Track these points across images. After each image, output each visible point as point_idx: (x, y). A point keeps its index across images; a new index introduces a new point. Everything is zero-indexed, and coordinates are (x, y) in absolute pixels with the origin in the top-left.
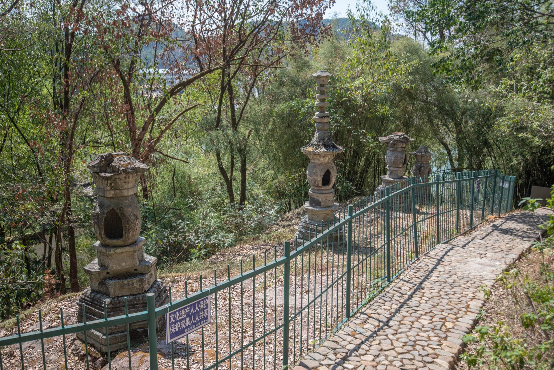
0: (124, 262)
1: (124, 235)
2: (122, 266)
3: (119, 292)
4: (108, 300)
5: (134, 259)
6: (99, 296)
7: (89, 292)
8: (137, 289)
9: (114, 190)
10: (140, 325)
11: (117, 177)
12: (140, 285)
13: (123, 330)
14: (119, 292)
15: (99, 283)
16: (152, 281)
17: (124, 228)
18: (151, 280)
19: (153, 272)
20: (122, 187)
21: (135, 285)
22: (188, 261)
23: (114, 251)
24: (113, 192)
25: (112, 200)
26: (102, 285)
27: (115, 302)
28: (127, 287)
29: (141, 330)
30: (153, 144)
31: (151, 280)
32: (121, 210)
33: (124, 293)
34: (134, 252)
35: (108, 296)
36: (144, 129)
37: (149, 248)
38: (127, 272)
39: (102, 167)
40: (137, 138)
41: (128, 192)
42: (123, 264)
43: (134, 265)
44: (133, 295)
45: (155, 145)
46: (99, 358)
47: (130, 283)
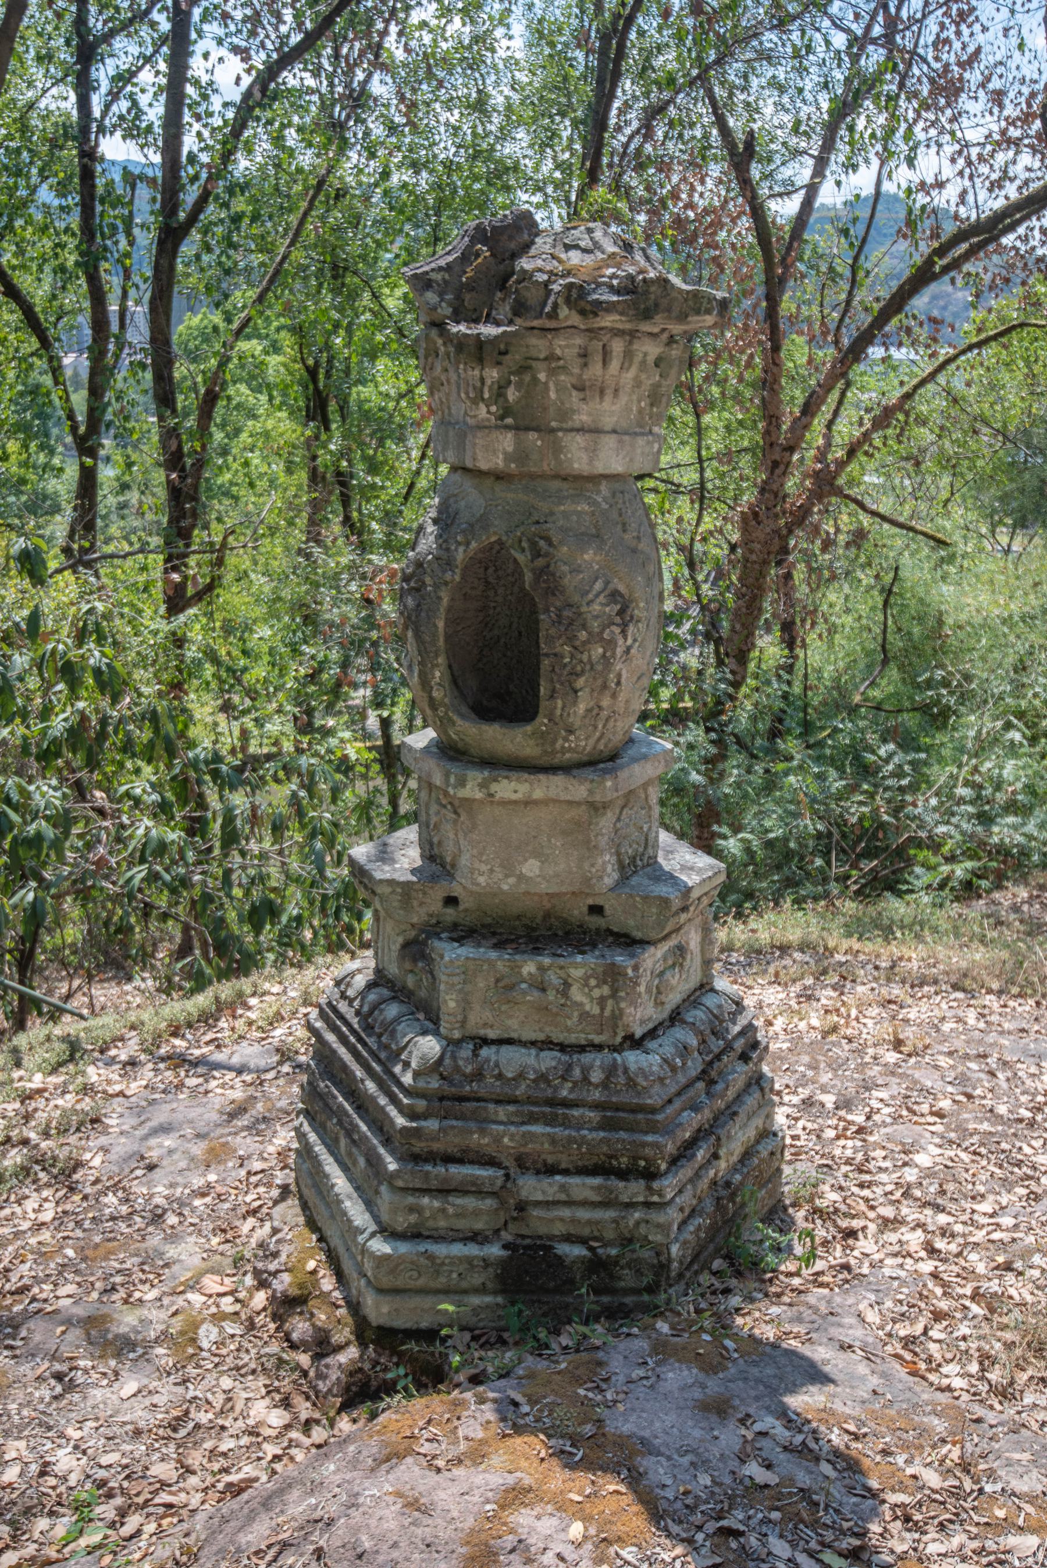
0: (537, 854)
1: (544, 704)
2: (521, 877)
3: (487, 1015)
4: (429, 1046)
5: (591, 848)
6: (392, 1010)
7: (360, 981)
8: (584, 1015)
9: (517, 428)
10: (574, 1221)
11: (538, 345)
12: (602, 1001)
13: (479, 1225)
14: (487, 1015)
15: (406, 945)
16: (679, 986)
17: (546, 663)
18: (674, 978)
19: (693, 939)
20: (564, 414)
21: (577, 994)
22: (899, 894)
23: (483, 785)
24: (507, 442)
25: (499, 487)
26: (415, 961)
27: (457, 1069)
28: (534, 996)
29: (578, 1251)
30: (833, 467)
31: (674, 978)
32: (537, 554)
33: (515, 1025)
34: (596, 808)
35: (432, 1023)
36: (809, 409)
37: (768, 823)
38: (547, 915)
39: (470, 287)
40: (782, 441)
41: (593, 451)
42: (531, 868)
43: (587, 881)
44: (563, 1048)
45: (837, 473)
46: (340, 1348)
47: (553, 978)
